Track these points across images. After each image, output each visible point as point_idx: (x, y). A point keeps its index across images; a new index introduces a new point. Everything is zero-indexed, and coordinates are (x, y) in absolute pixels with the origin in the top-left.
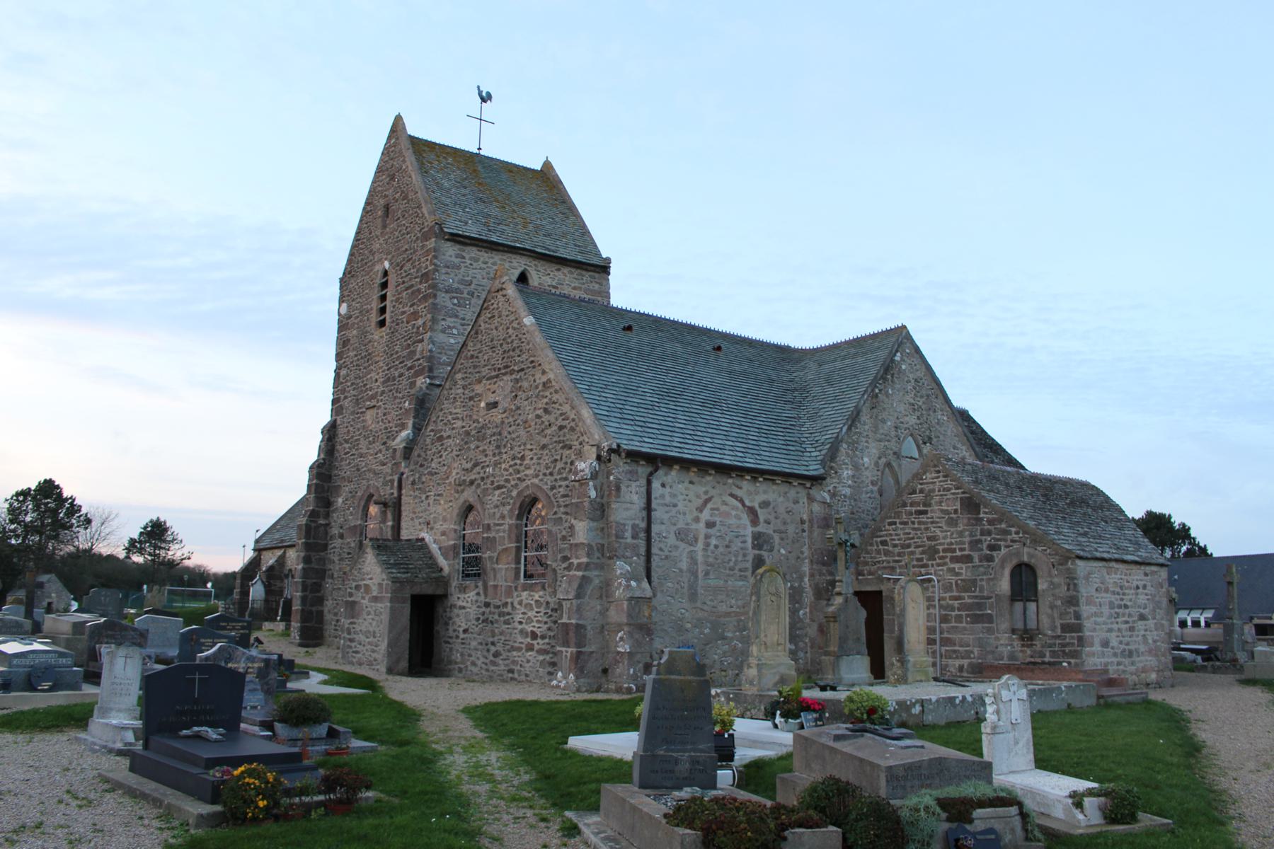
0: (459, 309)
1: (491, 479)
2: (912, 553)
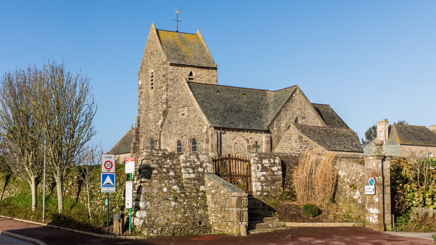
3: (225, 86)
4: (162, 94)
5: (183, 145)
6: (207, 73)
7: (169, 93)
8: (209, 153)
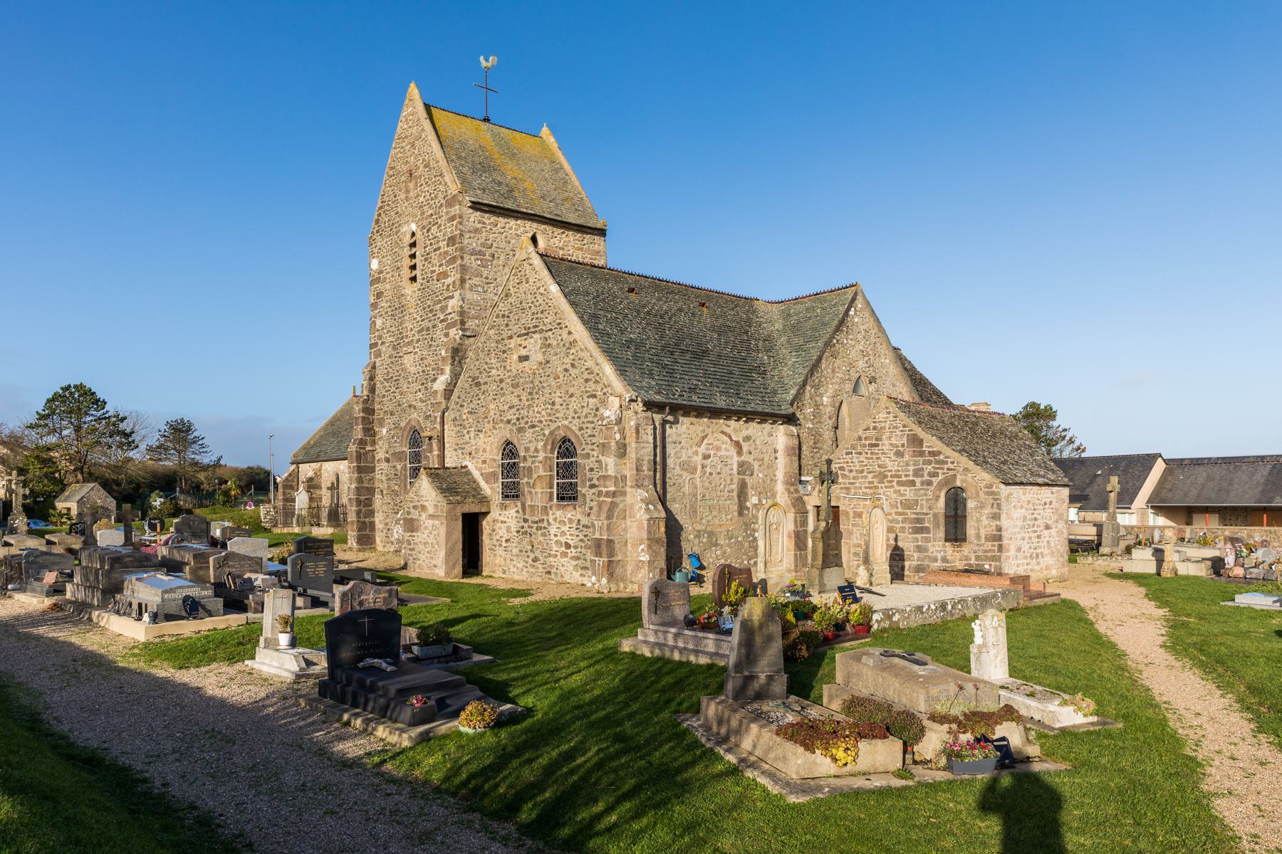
0: (483, 269)
1: (526, 419)
2: (866, 477)
4: (446, 295)
5: (525, 457)
6: (580, 243)
7: (469, 295)
8: (628, 489)
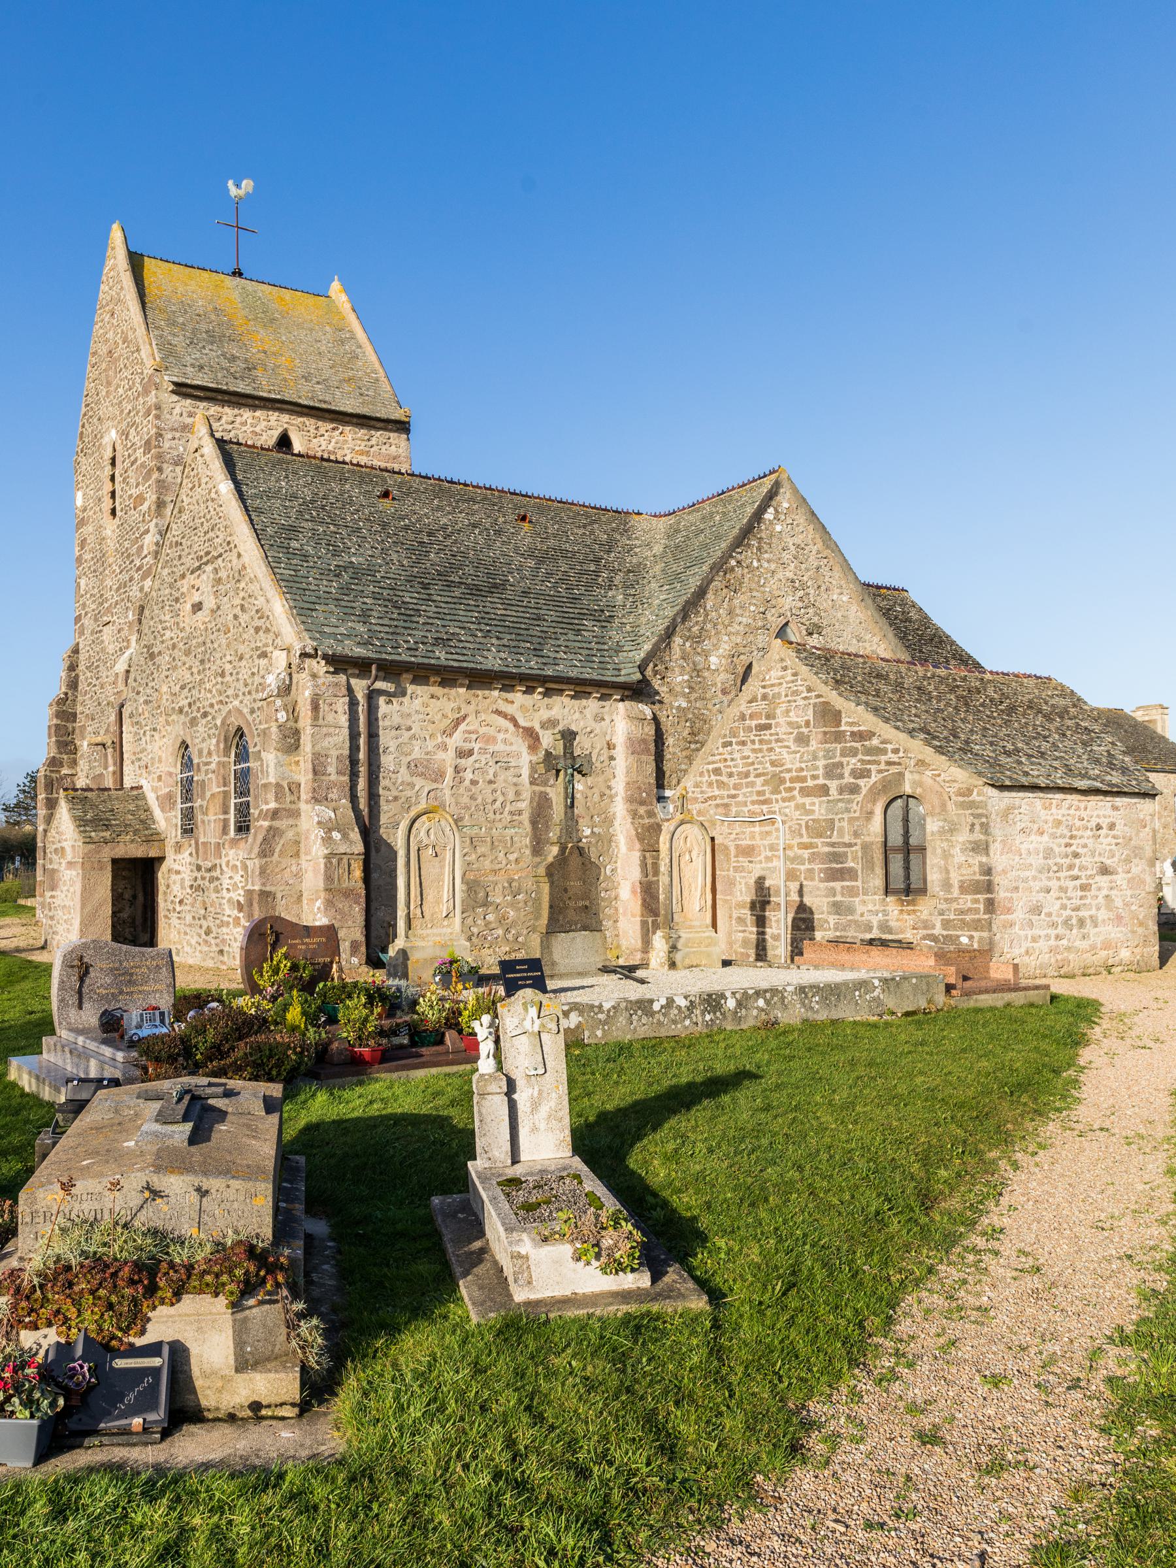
3: (427, 477)
5: (198, 764)
6: (364, 444)
8: (303, 806)
